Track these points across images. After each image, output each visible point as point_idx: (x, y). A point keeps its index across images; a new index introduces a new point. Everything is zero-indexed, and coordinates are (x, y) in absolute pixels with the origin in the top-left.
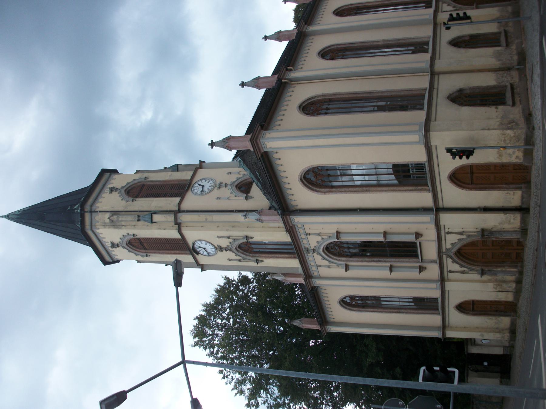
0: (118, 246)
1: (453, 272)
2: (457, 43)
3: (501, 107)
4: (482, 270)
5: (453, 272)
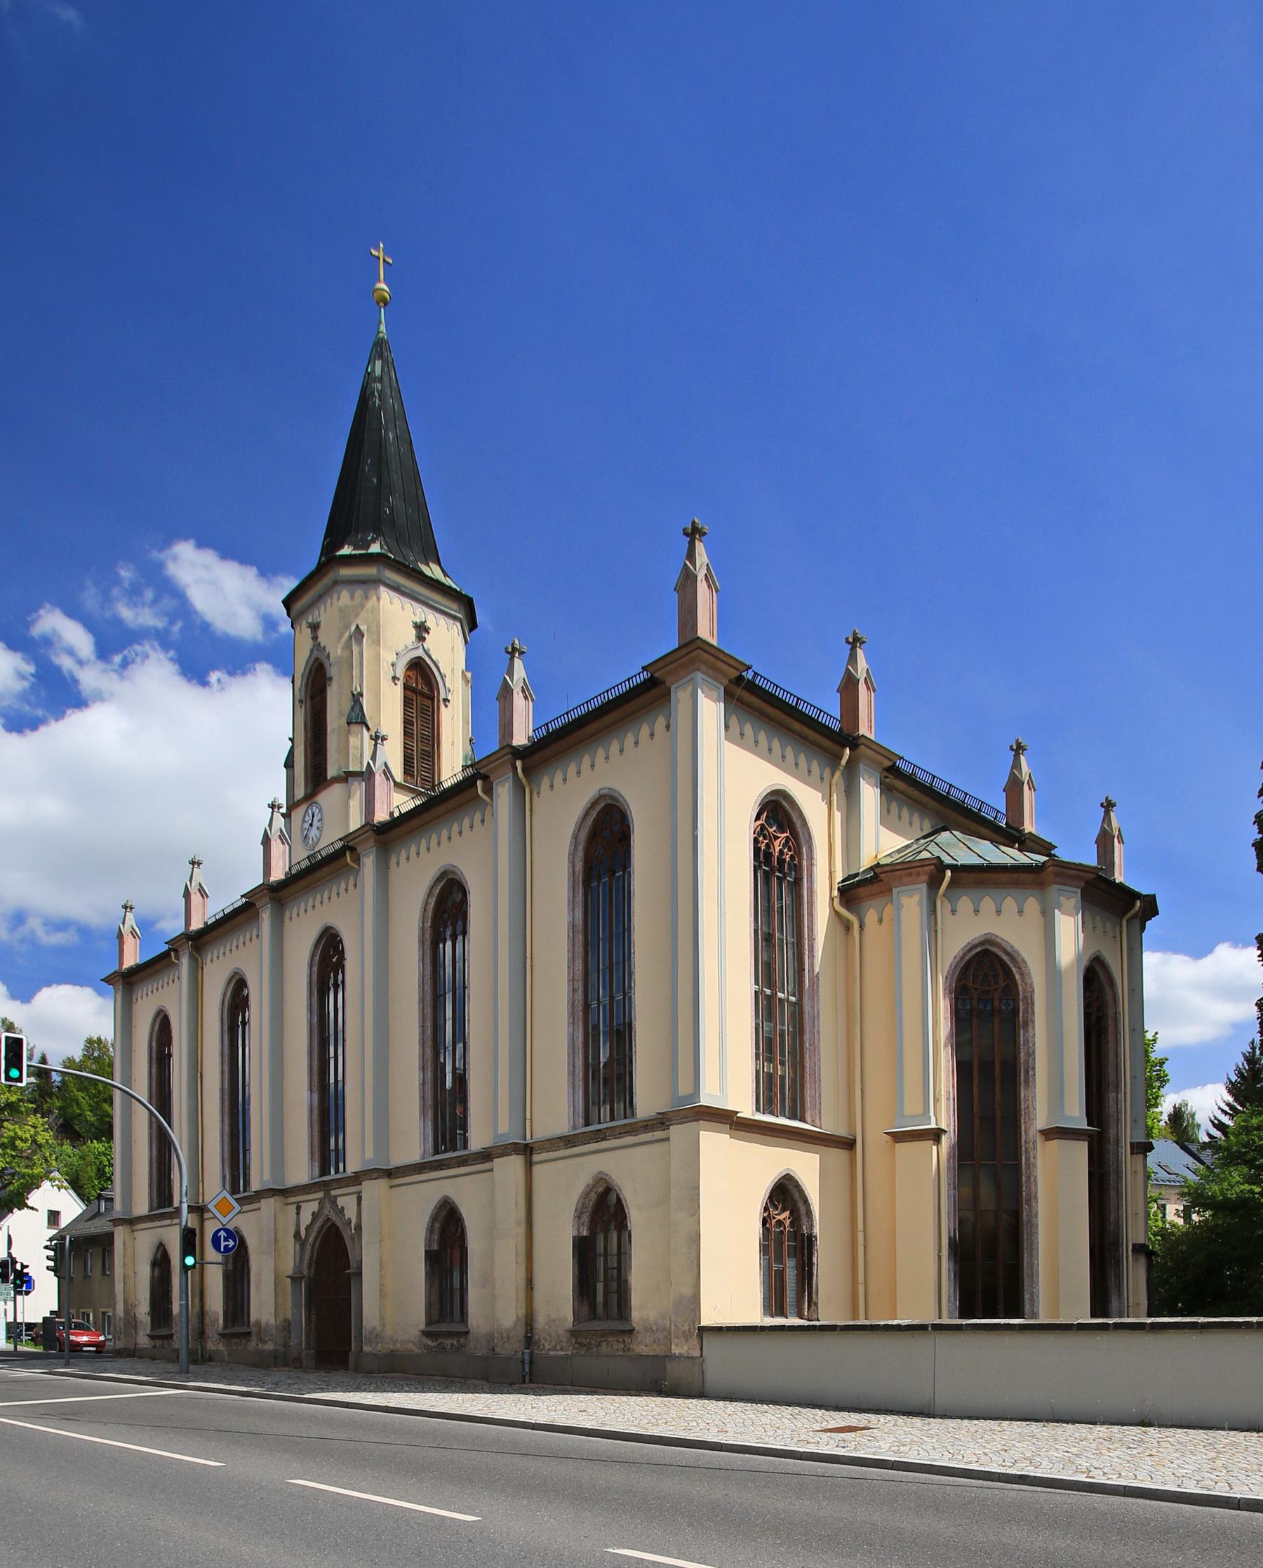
0: (315, 638)
1: (298, 1214)
2: (785, 1193)
3: (149, 1318)
4: (301, 1278)
5: (298, 1214)
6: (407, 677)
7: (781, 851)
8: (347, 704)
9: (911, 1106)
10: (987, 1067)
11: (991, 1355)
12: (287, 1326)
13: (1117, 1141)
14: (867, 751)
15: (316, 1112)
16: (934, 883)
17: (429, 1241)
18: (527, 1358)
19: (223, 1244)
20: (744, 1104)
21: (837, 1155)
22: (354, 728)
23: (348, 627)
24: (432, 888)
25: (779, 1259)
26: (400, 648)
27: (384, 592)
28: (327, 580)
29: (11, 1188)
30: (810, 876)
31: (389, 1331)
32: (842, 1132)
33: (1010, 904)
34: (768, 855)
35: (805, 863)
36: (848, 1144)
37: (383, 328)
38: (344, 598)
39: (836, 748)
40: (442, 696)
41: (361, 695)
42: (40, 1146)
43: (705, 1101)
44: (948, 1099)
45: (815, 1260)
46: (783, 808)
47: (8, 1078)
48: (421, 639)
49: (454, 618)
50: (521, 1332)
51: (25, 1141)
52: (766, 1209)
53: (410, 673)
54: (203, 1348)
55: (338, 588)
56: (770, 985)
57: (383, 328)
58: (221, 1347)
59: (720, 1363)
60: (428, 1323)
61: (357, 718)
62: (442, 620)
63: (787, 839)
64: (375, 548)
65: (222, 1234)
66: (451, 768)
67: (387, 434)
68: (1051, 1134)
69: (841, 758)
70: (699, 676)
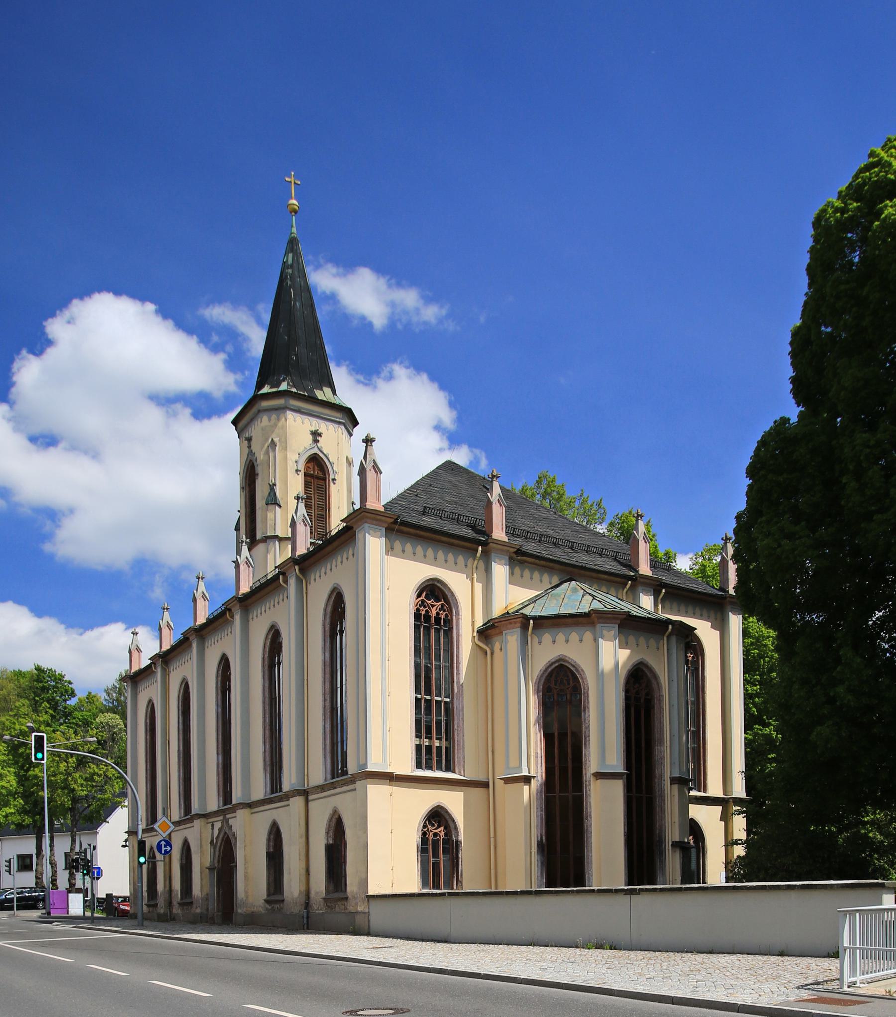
0: (249, 447)
6: (307, 468)
7: (437, 613)
8: (267, 490)
9: (513, 763)
10: (563, 735)
11: (566, 908)
12: (206, 899)
13: (661, 776)
14: (495, 545)
15: (220, 766)
16: (525, 627)
17: (268, 846)
18: (305, 915)
19: (163, 849)
20: (405, 765)
21: (477, 793)
22: (270, 507)
23: (267, 440)
24: (267, 635)
25: (435, 854)
26: (301, 450)
27: (289, 414)
28: (254, 410)
29: (91, 808)
30: (458, 626)
31: (251, 900)
32: (482, 778)
33: (574, 636)
34: (427, 617)
35: (454, 618)
36: (486, 785)
37: (294, 230)
38: (264, 421)
39: (475, 546)
40: (331, 477)
41: (275, 484)
42: (110, 779)
43: (370, 768)
44: (536, 757)
45: (460, 855)
46: (438, 587)
47: (36, 758)
48: (316, 441)
49: (340, 423)
50: (303, 900)
51: (99, 776)
52: (424, 827)
53: (309, 465)
54: (171, 912)
55: (261, 415)
56: (428, 692)
57: (294, 230)
58: (179, 912)
59: (378, 915)
60: (268, 895)
61: (273, 501)
62: (331, 426)
63: (442, 605)
64: (284, 387)
65: (163, 843)
66: (335, 524)
67: (295, 304)
68: (599, 776)
69: (477, 551)
70: (367, 526)
